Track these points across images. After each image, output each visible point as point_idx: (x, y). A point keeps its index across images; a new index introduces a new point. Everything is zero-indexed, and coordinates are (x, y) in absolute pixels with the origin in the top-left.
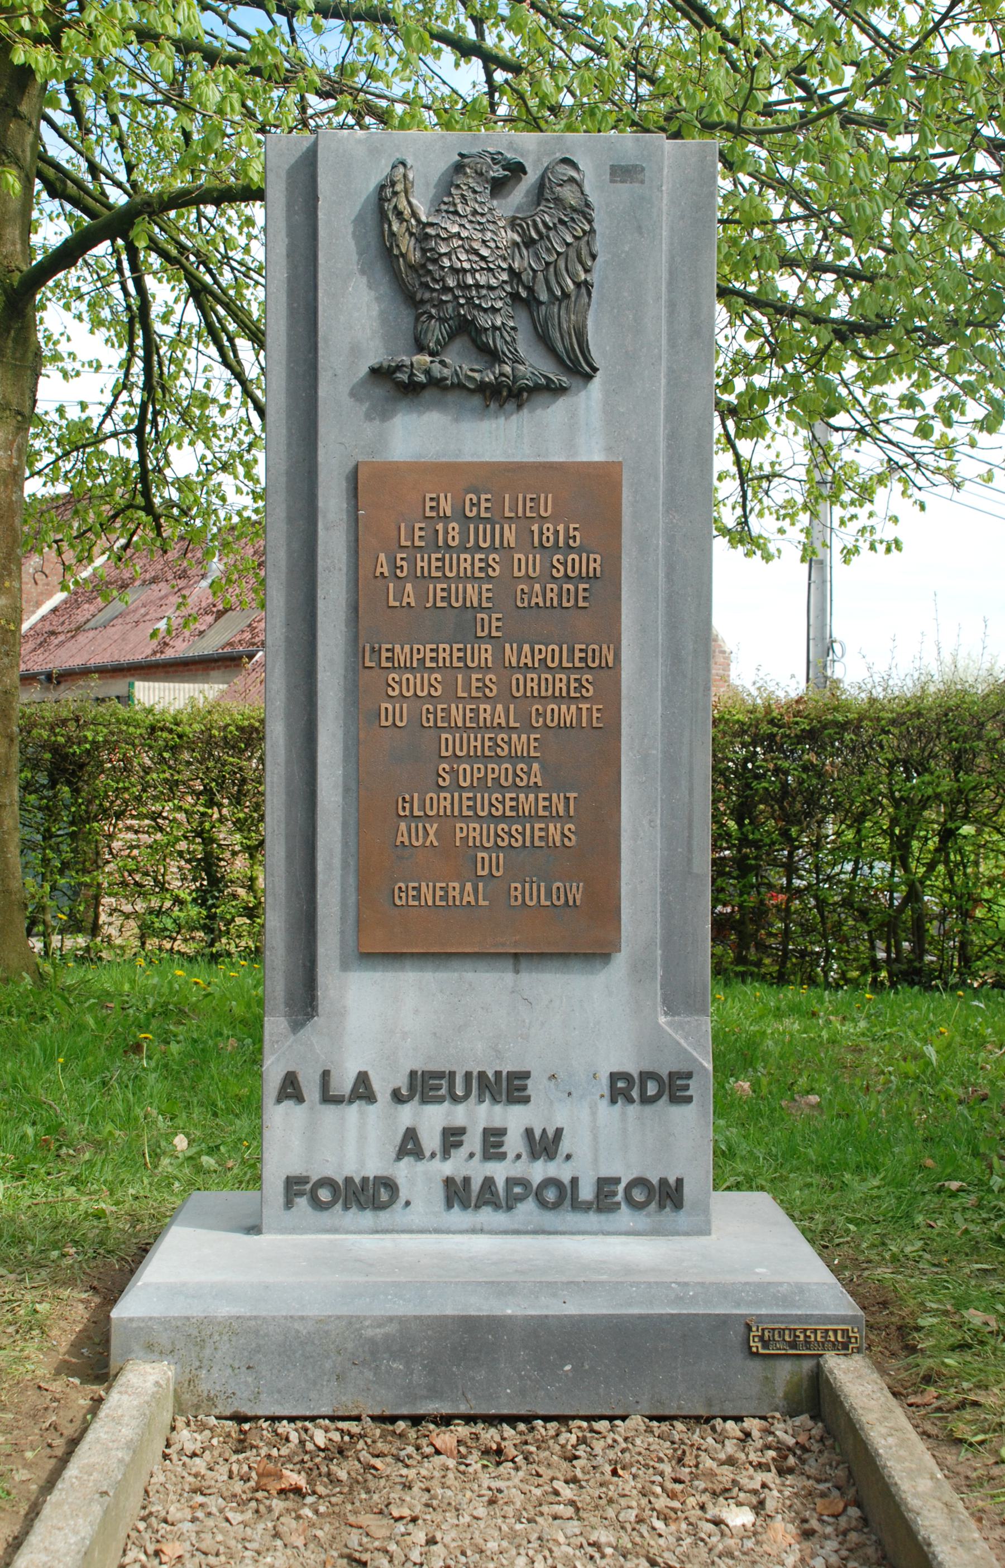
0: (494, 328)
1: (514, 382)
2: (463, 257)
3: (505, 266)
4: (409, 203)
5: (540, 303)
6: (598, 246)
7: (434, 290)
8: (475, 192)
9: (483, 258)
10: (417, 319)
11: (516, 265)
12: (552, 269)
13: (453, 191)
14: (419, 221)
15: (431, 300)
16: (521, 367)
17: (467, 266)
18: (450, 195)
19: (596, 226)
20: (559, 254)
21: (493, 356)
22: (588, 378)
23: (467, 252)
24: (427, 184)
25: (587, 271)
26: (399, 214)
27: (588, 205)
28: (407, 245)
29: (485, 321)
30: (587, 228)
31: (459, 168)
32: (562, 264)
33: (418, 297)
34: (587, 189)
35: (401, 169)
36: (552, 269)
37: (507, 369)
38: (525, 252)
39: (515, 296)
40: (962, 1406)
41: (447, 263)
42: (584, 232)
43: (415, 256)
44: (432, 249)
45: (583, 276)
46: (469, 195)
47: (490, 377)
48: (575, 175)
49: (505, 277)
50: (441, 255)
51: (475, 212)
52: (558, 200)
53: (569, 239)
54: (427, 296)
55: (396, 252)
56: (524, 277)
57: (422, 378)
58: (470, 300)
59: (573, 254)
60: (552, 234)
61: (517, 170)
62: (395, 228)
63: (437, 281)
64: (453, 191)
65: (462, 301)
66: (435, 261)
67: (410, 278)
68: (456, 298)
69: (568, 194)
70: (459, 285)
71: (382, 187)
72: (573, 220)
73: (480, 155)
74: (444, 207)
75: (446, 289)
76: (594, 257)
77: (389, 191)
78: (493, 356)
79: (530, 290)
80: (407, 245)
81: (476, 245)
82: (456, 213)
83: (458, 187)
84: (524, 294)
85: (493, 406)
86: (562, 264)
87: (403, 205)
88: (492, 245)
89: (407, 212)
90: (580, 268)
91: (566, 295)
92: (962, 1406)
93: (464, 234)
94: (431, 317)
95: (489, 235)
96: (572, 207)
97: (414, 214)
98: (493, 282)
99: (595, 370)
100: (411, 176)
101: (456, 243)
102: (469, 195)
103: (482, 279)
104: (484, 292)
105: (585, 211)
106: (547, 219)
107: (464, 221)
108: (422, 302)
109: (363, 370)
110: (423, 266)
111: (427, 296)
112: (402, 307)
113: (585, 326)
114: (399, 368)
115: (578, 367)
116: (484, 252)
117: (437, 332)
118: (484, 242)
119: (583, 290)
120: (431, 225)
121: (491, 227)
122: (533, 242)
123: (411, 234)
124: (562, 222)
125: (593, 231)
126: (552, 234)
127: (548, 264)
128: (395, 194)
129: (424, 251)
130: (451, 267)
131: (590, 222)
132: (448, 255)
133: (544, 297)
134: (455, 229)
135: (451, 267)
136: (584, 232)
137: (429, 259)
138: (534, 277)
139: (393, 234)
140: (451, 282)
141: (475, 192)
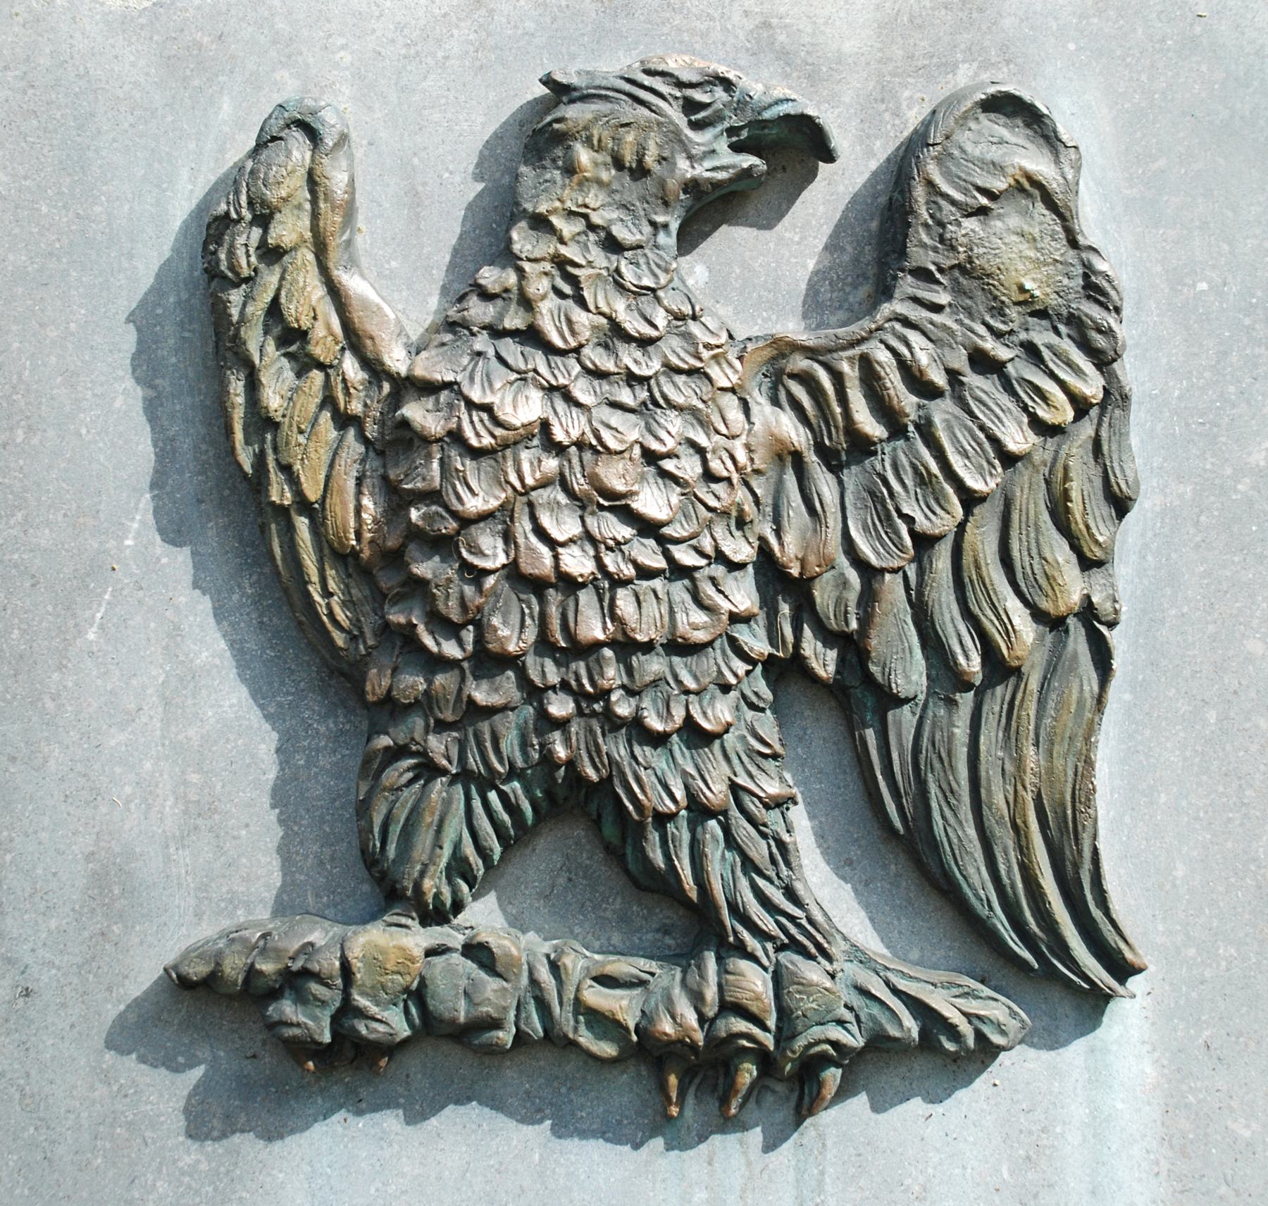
0: (700, 811)
1: (785, 1033)
2: (564, 526)
3: (740, 550)
4: (335, 292)
5: (889, 700)
6: (1143, 449)
7: (440, 663)
8: (613, 245)
9: (648, 528)
10: (374, 766)
11: (790, 550)
12: (942, 561)
13: (522, 240)
14: (375, 368)
15: (426, 703)
16: (813, 972)
17: (578, 563)
18: (507, 257)
19: (1129, 370)
20: (970, 500)
21: (699, 928)
22: (1094, 1003)
23: (580, 503)
24: (414, 200)
25: (1087, 564)
26: (292, 338)
27: (1094, 290)
28: (326, 464)
29: (658, 779)
30: (1092, 387)
31: (541, 136)
32: (983, 540)
33: (377, 682)
34: (1090, 229)
35: (298, 150)
36: (942, 561)
37: (754, 982)
38: (825, 484)
39: (785, 671)
40: (691, 372)
41: (492, 553)
42: (1081, 406)
43: (358, 513)
44: (433, 496)
45: (1073, 587)
46: (591, 260)
47: (681, 1020)
48: (1039, 164)
49: (742, 594)
50: (466, 522)
51: (616, 333)
52: (969, 274)
53: (1017, 438)
54: (413, 683)
55: (279, 493)
56: (823, 595)
57: (395, 1022)
58: (592, 701)
59: (1032, 501)
60: (942, 412)
61: (795, 146)
62: (273, 400)
63: (452, 630)
64: (522, 240)
65: (560, 707)
66: (443, 545)
67: (331, 598)
68: (534, 693)
69: (1015, 249)
70: (544, 645)
71: (215, 229)
72: (1031, 351)
73: (633, 90)
74: (479, 311)
75: (489, 661)
76: (1120, 505)
77: (247, 239)
78: (699, 928)
79: (853, 648)
80: (326, 464)
81: (615, 476)
82: (532, 336)
83: (541, 223)
84: (823, 661)
85: (690, 1113)
86: (983, 540)
87: (307, 300)
88: (689, 467)
89: (325, 334)
90: (1061, 552)
91: (1000, 669)
92: (691, 372)
93: (568, 427)
94: (428, 770)
95: (673, 427)
96: (1027, 302)
97: (354, 339)
98: (694, 624)
99: (1123, 969)
100: (337, 180)
101: (532, 464)
102: (591, 260)
103: (643, 614)
104: (654, 665)
105: (1085, 316)
106: (923, 354)
107: (568, 373)
108: (392, 708)
109: (143, 973)
110: (395, 558)
111: (413, 683)
112: (312, 708)
113: (1083, 795)
114: (295, 980)
115: (1057, 958)
116: (653, 501)
117: (456, 826)
118: (651, 457)
119: (1078, 641)
120: (429, 388)
121: (682, 391)
122: (862, 446)
123: (344, 421)
124: (982, 362)
125: (1115, 397)
126: (942, 412)
127: (924, 542)
128: (272, 254)
129: (397, 500)
130: (513, 572)
131: (1103, 361)
132: (501, 518)
133: (910, 673)
134: (527, 408)
135: (513, 572)
136: (1081, 406)
137: (414, 534)
138: (869, 597)
139: (261, 423)
140: (511, 634)
141: (613, 245)
